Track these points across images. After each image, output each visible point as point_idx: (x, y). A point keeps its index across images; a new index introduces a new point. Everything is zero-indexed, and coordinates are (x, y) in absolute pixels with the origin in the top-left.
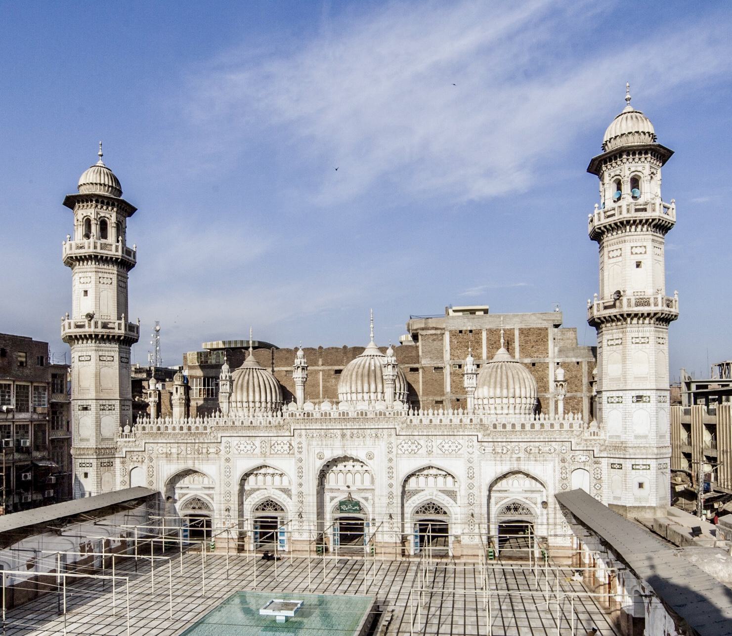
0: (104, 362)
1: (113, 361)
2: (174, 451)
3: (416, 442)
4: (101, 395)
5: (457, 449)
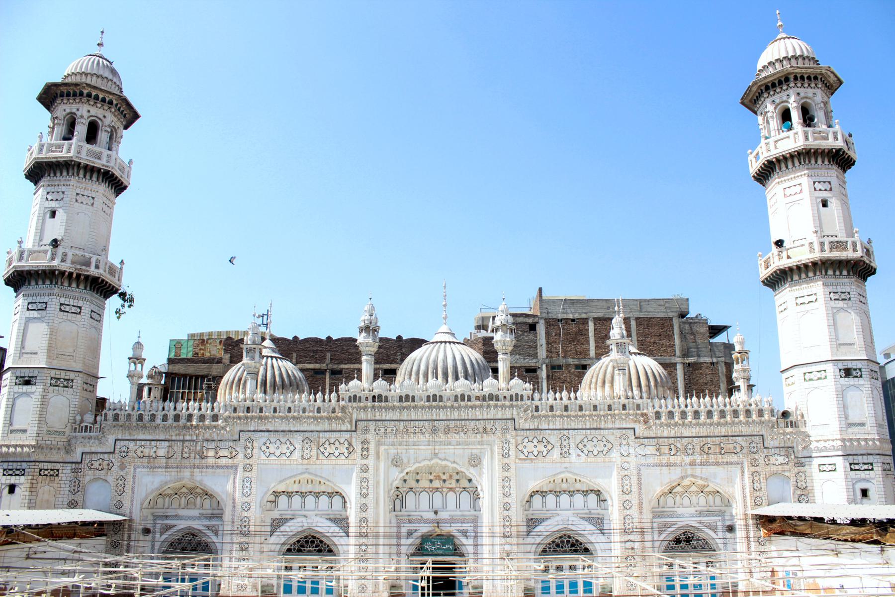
0: (66, 314)
1: (80, 313)
2: (161, 452)
3: (544, 440)
4: (55, 362)
5: (605, 449)
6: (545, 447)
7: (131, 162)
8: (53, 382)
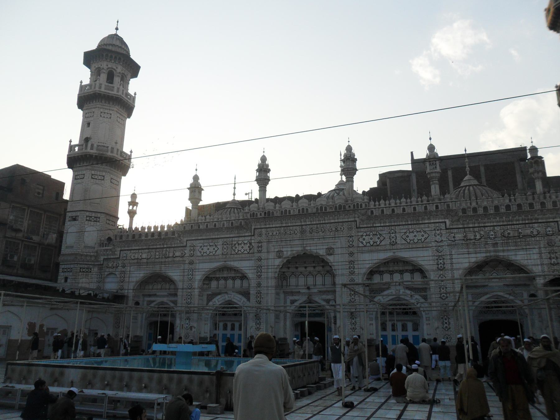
1: (103, 180)
6: (379, 238)
7: (135, 94)
8: (88, 218)
